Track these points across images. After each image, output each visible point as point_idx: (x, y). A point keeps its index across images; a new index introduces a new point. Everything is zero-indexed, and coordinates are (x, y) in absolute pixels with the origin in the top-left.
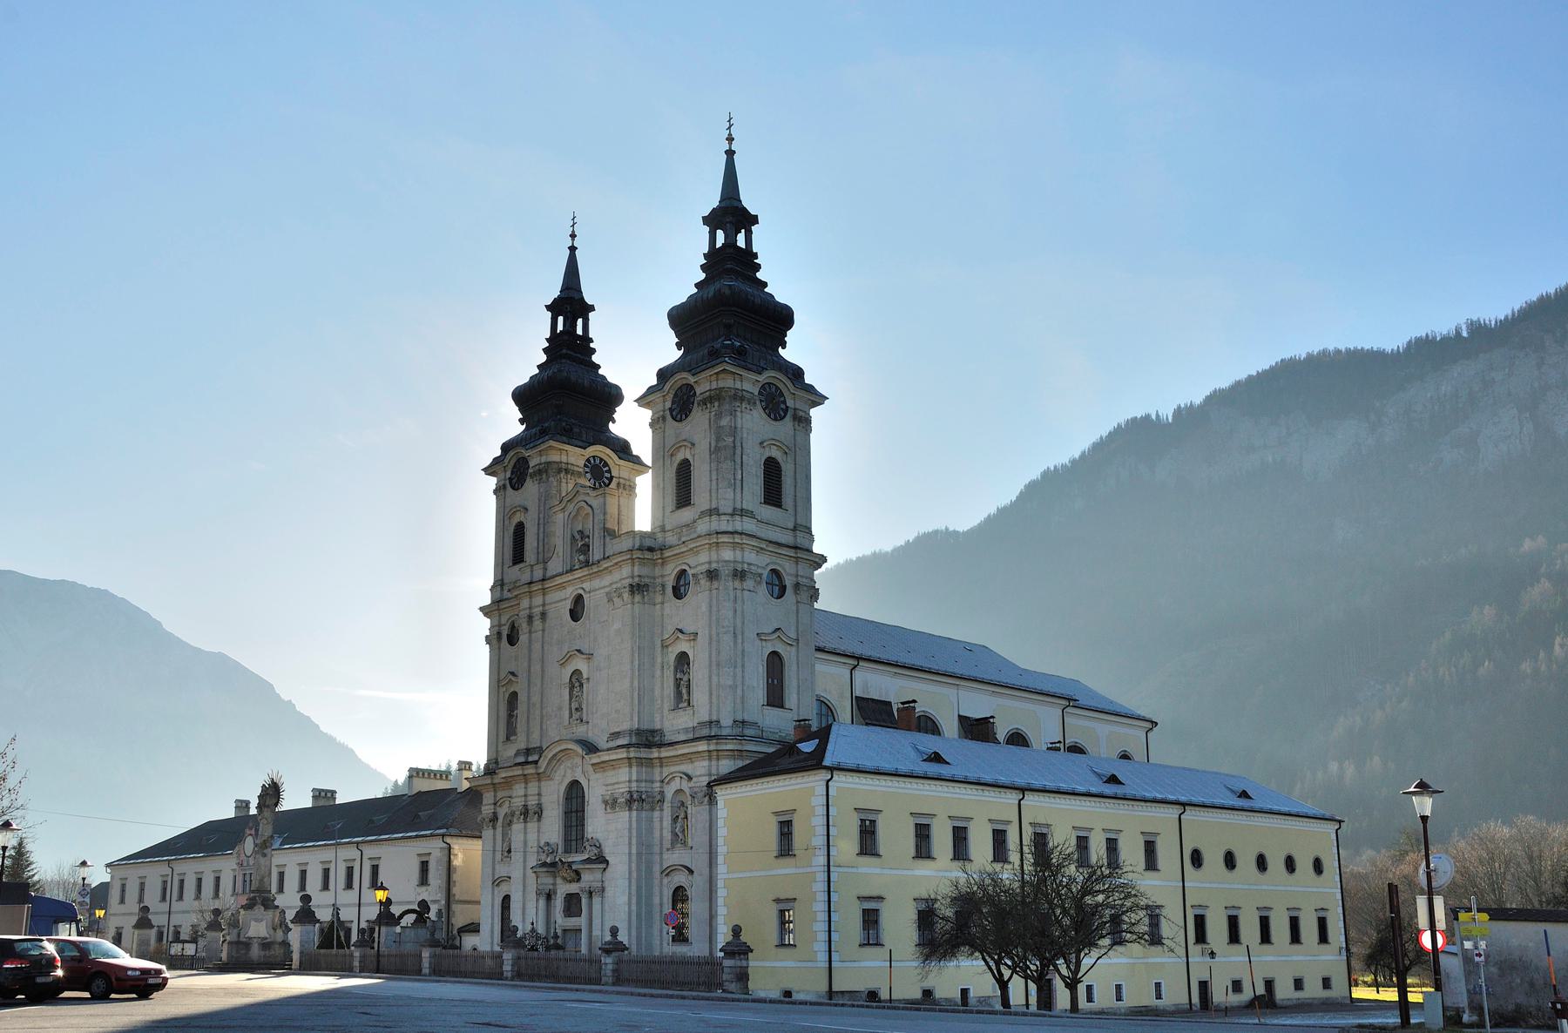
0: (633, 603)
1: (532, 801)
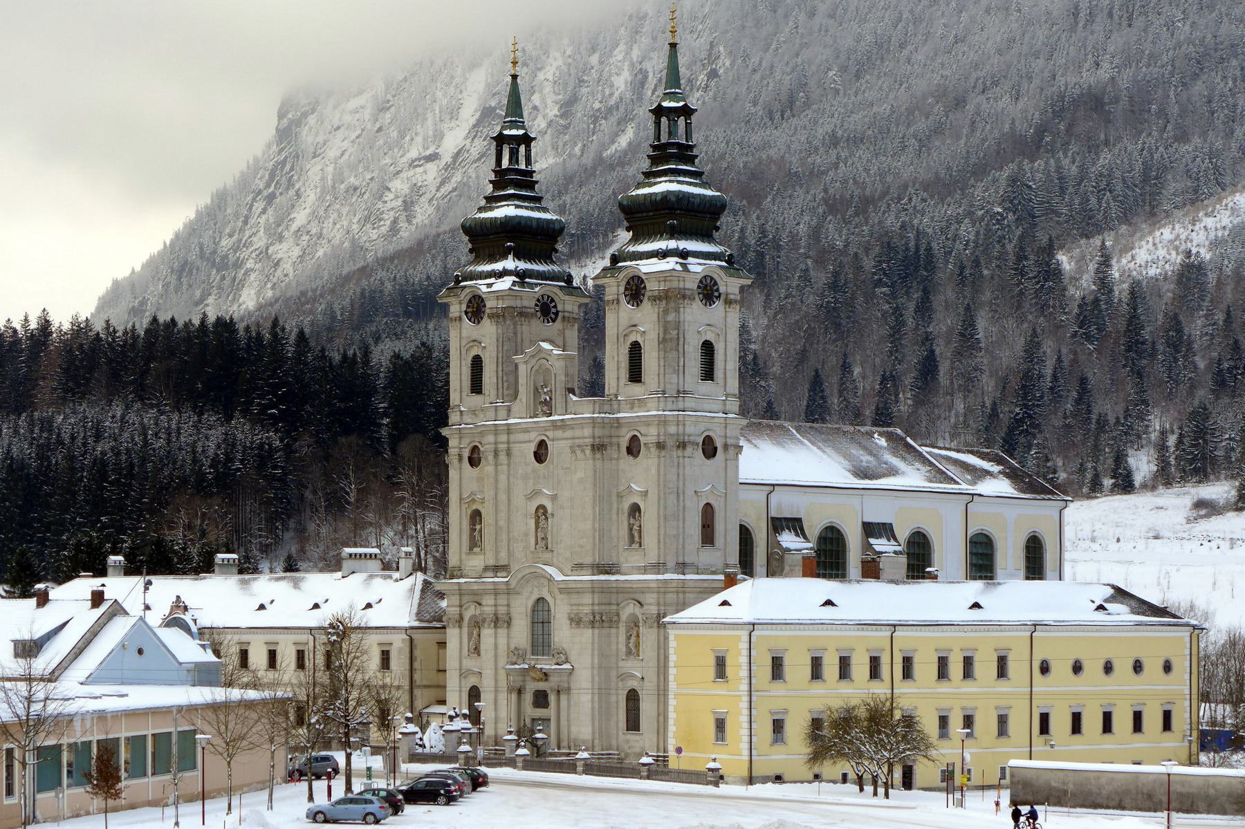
0: (594, 459)
1: (502, 610)
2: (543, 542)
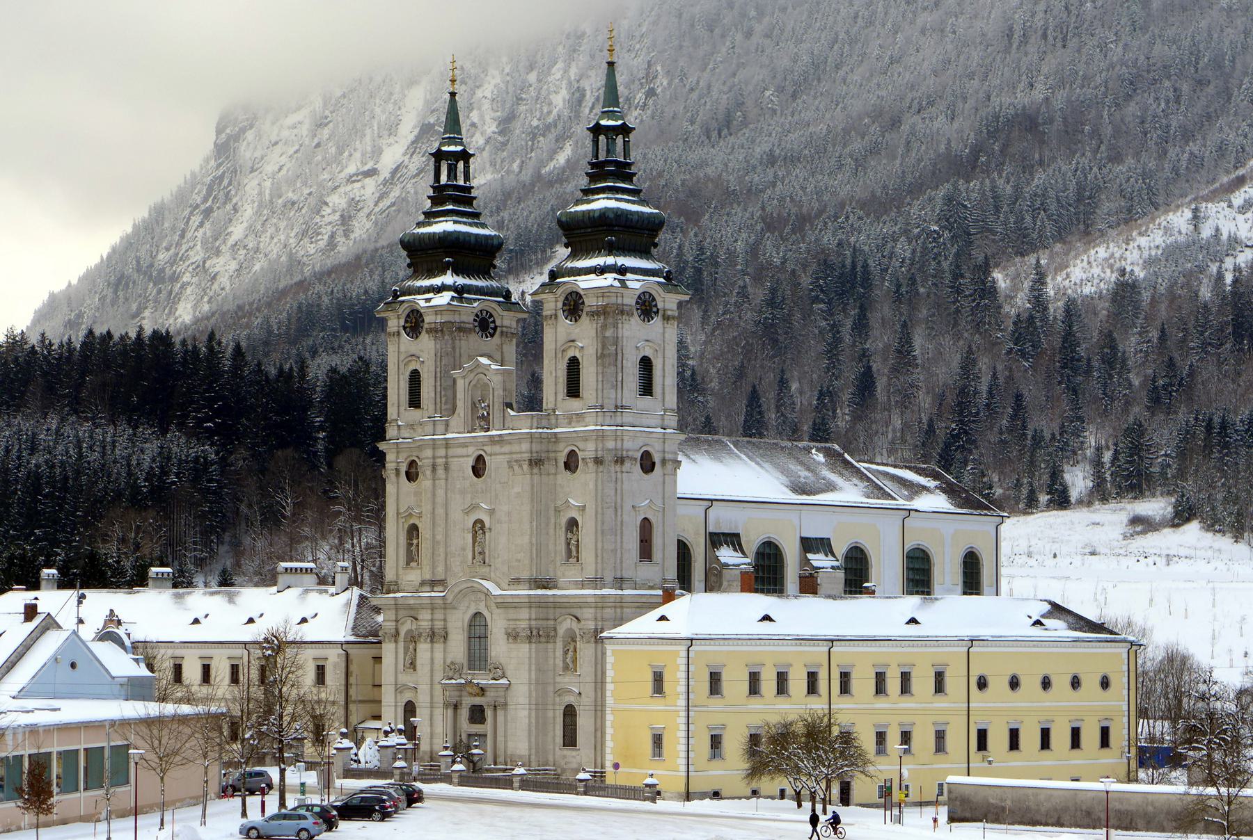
0: (532, 474)
1: (439, 625)
2: (481, 557)
